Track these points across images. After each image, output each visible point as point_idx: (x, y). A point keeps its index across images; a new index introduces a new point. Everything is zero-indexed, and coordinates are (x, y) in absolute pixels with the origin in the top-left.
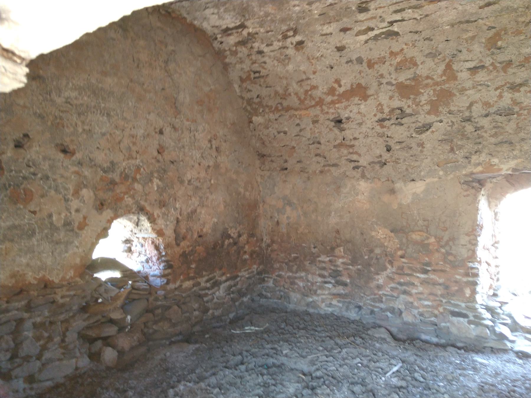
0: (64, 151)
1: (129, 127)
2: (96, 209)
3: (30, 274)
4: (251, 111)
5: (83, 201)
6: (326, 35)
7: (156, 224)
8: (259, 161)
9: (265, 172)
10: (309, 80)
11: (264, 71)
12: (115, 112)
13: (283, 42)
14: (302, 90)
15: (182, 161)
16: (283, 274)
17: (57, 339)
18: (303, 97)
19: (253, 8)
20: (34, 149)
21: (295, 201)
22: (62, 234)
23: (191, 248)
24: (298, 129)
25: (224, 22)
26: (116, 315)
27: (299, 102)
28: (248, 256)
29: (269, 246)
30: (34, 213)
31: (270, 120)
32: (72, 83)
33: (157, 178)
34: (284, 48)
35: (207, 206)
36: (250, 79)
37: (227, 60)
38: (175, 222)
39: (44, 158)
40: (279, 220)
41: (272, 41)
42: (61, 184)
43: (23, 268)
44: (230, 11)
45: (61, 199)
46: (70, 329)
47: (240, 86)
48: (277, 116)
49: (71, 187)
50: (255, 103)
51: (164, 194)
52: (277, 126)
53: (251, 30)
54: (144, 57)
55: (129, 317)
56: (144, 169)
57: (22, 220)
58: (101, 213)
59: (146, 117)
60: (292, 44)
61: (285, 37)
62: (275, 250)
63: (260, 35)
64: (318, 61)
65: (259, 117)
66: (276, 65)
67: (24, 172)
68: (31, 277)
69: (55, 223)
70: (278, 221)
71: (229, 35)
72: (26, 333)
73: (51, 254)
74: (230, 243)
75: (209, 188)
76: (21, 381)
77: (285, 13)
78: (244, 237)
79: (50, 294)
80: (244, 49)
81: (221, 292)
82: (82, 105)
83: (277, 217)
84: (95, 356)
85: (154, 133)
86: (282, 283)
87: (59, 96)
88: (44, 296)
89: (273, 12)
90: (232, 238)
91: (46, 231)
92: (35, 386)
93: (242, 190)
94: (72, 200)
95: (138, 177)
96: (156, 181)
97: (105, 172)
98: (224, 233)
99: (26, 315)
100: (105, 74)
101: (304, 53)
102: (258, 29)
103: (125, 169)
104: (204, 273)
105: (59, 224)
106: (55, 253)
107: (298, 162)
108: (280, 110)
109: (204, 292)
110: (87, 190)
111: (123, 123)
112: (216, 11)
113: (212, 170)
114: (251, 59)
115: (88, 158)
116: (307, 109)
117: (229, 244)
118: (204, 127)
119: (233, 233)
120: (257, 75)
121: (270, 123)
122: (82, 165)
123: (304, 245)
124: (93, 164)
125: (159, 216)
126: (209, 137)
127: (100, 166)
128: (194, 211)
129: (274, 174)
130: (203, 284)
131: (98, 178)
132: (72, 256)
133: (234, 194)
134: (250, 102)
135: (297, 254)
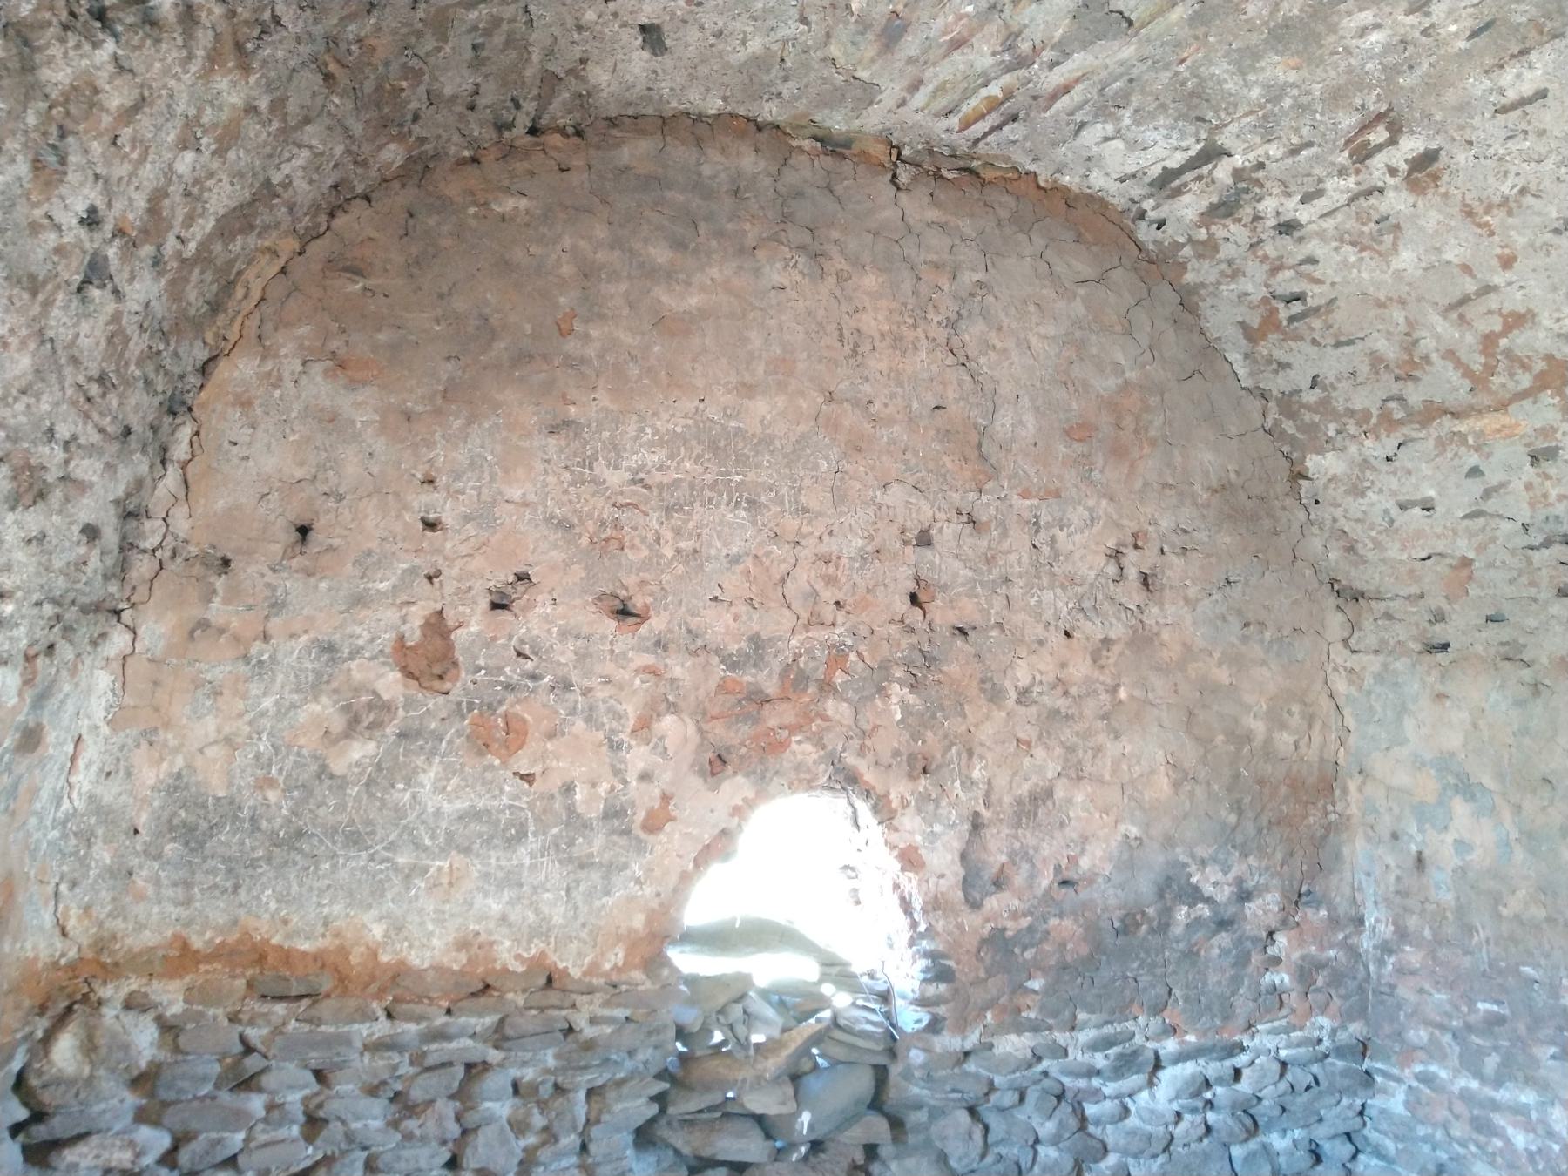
0: (623, 612)
1: (817, 534)
2: (701, 773)
3: (508, 943)
5: (660, 749)
6: (1523, 102)
7: (896, 830)
8: (1340, 617)
9: (1365, 658)
10: (1493, 296)
11: (1317, 289)
13: (1358, 172)
14: (1470, 338)
15: (999, 625)
16: (1443, 1074)
17: (570, 1140)
18: (1477, 362)
19: (1220, 82)
21: (1488, 781)
22: (599, 841)
23: (1025, 922)
24: (1476, 487)
25: (1151, 155)
26: (762, 1102)
27: (1467, 384)
28: (1287, 979)
29: (1386, 948)
30: (528, 778)
31: (1366, 464)
32: (653, 426)
33: (901, 682)
34: (1368, 193)
36: (1277, 327)
37: (1189, 277)
38: (967, 826)
39: (564, 634)
40: (1426, 853)
42: (604, 701)
43: (492, 925)
44: (1152, 116)
46: (605, 1117)
47: (1247, 356)
48: (1390, 445)
49: (630, 710)
50: (1308, 407)
51: (929, 734)
52: (1394, 483)
53: (1238, 161)
54: (873, 322)
55: (806, 1117)
56: (859, 654)
57: (494, 797)
58: (715, 788)
59: (873, 499)
60: (1393, 171)
61: (1363, 154)
62: (1413, 973)
64: (1510, 213)
65: (1329, 455)
66: (1352, 259)
67: (507, 670)
68: (508, 954)
69: (581, 809)
70: (1420, 853)
71: (1178, 192)
72: (488, 1104)
73: (563, 893)
75: (1105, 717)
79: (561, 1008)
80: (1232, 228)
81: (1165, 1093)
82: (676, 483)
83: (1419, 838)
86: (1442, 1114)
87: (616, 468)
88: (542, 1009)
89: (1292, 76)
90: (1209, 900)
91: (555, 830)
93: (1259, 727)
95: (839, 678)
97: (733, 666)
98: (1169, 878)
99: (494, 1056)
100: (748, 390)
101: (1446, 195)
102: (1261, 151)
103: (797, 657)
105: (594, 812)
106: (574, 894)
107: (1489, 619)
108: (1401, 423)
110: (674, 717)
111: (796, 522)
113: (1121, 654)
114: (1266, 257)
116: (1502, 406)
119: (1214, 882)
120: (1297, 308)
121: (1368, 473)
122: (665, 649)
123: (1528, 970)
125: (905, 804)
126: (1111, 543)
127: (717, 652)
128: (1042, 796)
129: (1400, 665)
130: (1077, 1056)
132: (624, 902)
133: (1221, 737)
135: (1499, 1003)
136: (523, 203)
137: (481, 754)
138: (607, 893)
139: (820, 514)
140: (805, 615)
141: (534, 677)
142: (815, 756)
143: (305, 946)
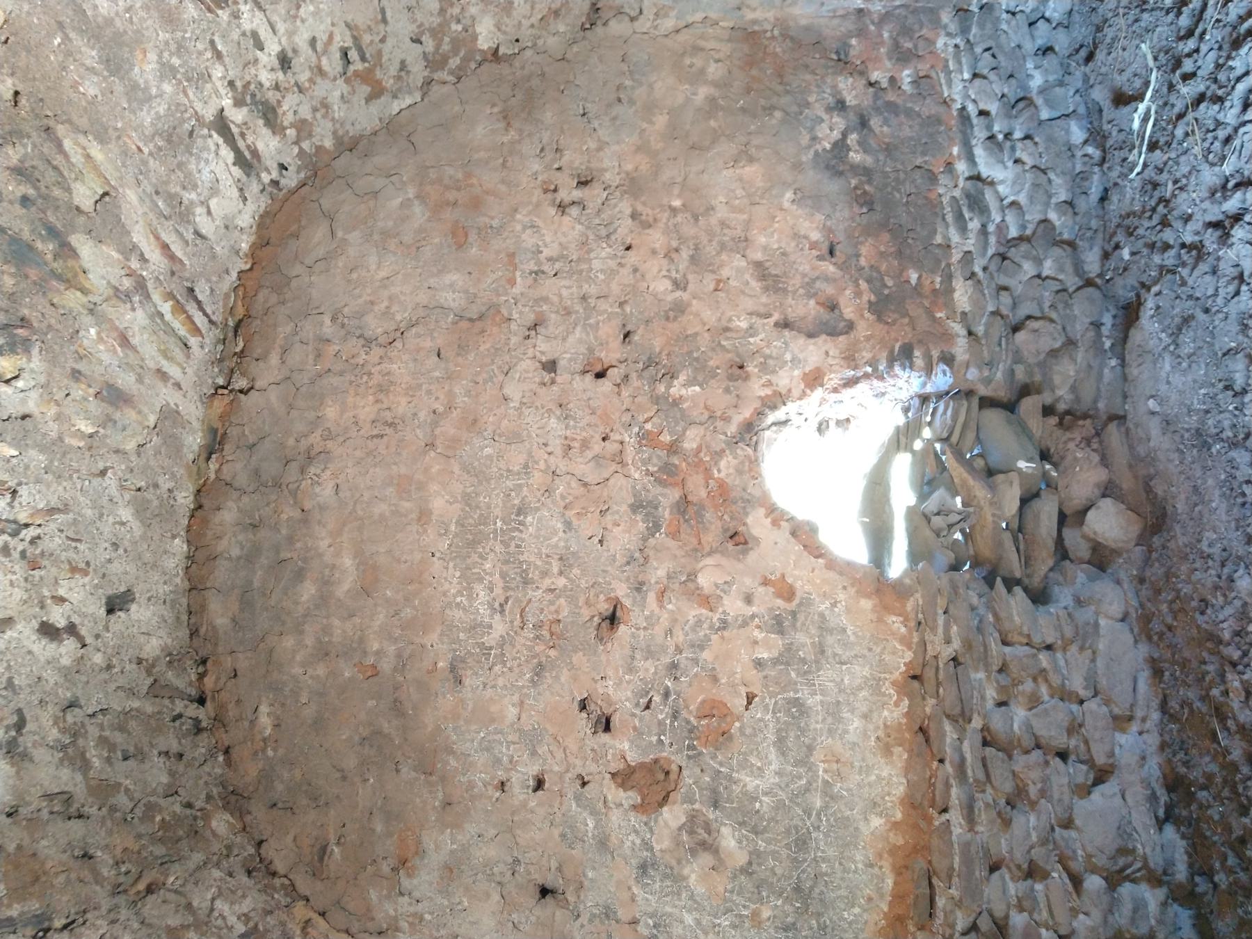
0: (612, 620)
2: (745, 552)
3: (886, 713)
4: (462, 54)
5: (726, 587)
7: (790, 391)
8: (612, 23)
11: (337, 38)
12: (513, 494)
15: (621, 304)
17: (1044, 659)
19: (158, 117)
20: (611, 691)
22: (801, 638)
23: (863, 285)
25: (223, 176)
28: (907, 72)
30: (750, 698)
33: (669, 386)
35: (748, 224)
36: (370, 71)
37: (328, 143)
38: (786, 333)
39: (631, 669)
41: (244, 34)
43: (871, 727)
44: (189, 175)
45: (723, 638)
47: (395, 97)
50: (438, 47)
51: (711, 363)
53: (227, 102)
54: (366, 409)
55: (1022, 464)
56: (646, 421)
59: (516, 409)
63: (232, 74)
67: (660, 717)
68: (894, 712)
71: (255, 153)
72: (1016, 726)
73: (844, 667)
74: (859, 143)
76: (1122, 738)
77: (142, 20)
78: (850, 89)
79: (937, 668)
80: (285, 108)
82: (503, 576)
84: (1101, 558)
85: (555, 388)
87: (490, 627)
89: (152, 56)
90: (845, 135)
91: (793, 675)
92: (1139, 714)
93: (703, 91)
94: (724, 612)
95: (666, 438)
96: (677, 389)
97: (657, 527)
98: (827, 167)
99: (977, 723)
100: (424, 516)
102: (219, 84)
104: (939, 239)
105: (778, 642)
106: (844, 658)
109: (992, 240)
111: (537, 474)
112: (200, 210)
114: (311, 80)
115: (627, 568)
117: (864, 146)
118: (525, 228)
119: (830, 130)
120: (353, 55)
122: (642, 584)
124: (639, 558)
126: (552, 211)
127: (645, 539)
128: (760, 269)
130: (971, 243)
131: (671, 543)
132: (851, 614)
133: (713, 123)
134: (435, 62)
136: (264, 709)
137: (731, 738)
138: (844, 630)
139: (530, 454)
140: (614, 467)
141: (666, 694)
142: (730, 458)
143: (890, 882)
